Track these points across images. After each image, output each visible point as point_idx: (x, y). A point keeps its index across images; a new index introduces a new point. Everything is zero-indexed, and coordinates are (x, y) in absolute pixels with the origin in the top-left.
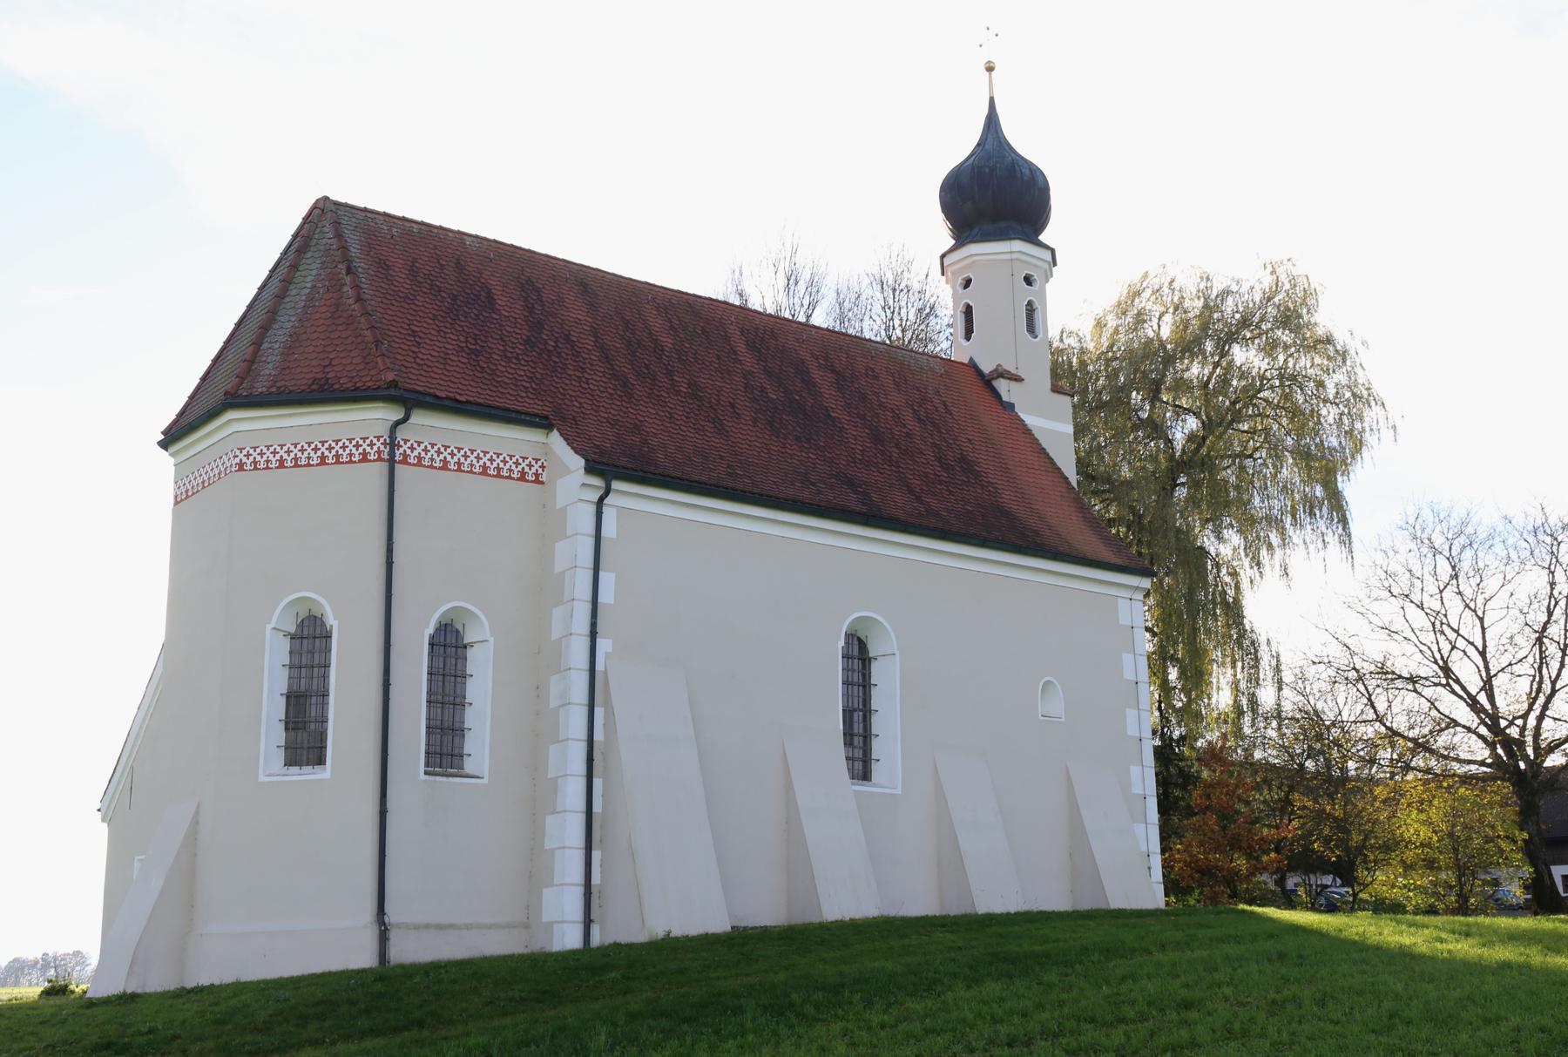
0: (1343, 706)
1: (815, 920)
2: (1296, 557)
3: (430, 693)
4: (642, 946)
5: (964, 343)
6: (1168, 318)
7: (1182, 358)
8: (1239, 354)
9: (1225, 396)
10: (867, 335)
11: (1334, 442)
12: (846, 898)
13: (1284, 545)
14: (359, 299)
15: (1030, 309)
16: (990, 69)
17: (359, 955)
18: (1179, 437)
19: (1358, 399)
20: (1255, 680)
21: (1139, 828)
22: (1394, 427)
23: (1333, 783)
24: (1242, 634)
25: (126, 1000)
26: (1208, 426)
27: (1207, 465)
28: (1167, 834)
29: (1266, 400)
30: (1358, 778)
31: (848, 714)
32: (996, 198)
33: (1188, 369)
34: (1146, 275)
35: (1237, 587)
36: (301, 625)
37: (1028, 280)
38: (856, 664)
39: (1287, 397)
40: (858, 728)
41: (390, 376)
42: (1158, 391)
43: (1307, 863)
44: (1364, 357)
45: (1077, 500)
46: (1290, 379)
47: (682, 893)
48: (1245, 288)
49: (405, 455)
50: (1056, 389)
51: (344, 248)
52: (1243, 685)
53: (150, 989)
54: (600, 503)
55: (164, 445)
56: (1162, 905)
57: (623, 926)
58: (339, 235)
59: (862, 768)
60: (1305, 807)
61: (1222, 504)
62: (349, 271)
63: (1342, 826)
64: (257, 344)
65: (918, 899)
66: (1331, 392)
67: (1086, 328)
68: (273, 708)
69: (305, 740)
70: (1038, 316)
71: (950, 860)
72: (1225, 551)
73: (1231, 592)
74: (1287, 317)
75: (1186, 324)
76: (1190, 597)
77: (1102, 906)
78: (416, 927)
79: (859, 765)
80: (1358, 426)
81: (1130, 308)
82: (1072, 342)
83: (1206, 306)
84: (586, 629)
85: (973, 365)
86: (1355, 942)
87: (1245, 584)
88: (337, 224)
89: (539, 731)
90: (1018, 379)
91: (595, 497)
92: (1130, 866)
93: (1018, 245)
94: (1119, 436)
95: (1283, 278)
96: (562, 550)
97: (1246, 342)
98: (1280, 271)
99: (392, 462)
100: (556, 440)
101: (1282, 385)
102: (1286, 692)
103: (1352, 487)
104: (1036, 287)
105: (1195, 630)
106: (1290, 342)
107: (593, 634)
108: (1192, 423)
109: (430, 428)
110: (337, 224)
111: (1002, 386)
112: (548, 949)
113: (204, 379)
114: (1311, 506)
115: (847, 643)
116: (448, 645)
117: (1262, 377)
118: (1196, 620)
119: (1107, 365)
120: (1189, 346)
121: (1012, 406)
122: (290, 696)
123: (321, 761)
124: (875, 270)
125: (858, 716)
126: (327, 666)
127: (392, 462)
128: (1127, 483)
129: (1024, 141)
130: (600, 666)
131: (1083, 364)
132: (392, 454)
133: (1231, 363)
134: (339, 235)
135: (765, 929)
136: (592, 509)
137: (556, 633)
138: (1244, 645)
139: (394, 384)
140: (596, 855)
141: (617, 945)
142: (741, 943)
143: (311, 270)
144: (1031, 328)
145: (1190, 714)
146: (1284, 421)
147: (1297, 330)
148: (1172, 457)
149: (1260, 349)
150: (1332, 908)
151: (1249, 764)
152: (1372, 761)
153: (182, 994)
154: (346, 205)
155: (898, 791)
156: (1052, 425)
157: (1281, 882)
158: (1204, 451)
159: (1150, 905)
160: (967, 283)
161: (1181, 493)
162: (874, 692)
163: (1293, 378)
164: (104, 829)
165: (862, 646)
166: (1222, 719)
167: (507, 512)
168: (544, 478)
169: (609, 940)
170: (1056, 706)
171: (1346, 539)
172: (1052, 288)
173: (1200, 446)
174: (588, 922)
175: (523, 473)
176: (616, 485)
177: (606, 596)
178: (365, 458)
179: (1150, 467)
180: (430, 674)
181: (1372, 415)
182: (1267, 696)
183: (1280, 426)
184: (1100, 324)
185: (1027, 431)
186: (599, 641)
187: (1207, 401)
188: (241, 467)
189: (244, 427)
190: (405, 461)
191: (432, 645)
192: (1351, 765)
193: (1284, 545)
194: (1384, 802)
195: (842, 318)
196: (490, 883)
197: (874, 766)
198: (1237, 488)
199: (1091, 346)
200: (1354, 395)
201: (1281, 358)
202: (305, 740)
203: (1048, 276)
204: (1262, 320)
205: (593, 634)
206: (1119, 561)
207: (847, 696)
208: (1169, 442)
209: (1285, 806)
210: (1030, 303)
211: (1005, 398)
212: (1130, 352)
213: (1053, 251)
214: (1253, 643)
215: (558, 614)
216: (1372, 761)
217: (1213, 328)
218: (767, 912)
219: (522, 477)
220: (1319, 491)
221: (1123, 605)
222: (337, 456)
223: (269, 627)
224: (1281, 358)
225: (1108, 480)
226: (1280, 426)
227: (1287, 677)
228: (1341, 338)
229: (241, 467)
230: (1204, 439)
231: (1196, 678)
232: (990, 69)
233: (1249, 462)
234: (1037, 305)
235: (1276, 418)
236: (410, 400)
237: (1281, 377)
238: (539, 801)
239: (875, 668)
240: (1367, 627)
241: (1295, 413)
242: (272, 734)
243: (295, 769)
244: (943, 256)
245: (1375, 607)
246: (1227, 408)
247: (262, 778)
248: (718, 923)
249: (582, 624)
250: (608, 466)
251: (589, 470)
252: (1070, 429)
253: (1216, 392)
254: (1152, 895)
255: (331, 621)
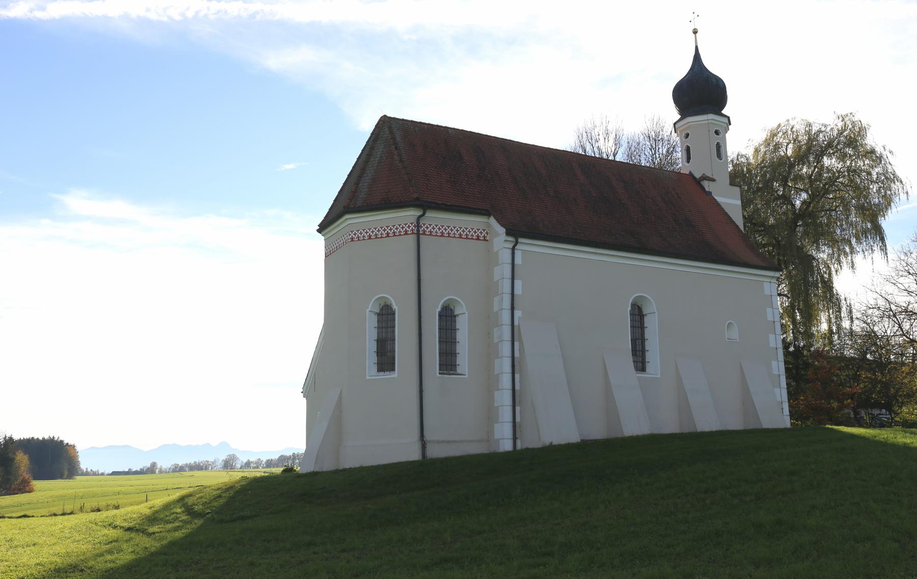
0: (886, 328)
1: (620, 436)
2: (858, 259)
3: (440, 338)
4: (539, 449)
5: (687, 164)
6: (791, 146)
7: (798, 165)
8: (827, 161)
9: (820, 181)
10: (643, 163)
11: (877, 200)
12: (634, 424)
13: (851, 253)
14: (401, 161)
15: (718, 146)
16: (695, 32)
17: (414, 455)
18: (798, 203)
19: (889, 178)
20: (839, 318)
21: (777, 390)
22: (907, 193)
23: (881, 365)
24: (832, 295)
25: (314, 474)
26: (812, 197)
27: (813, 215)
28: (792, 395)
29: (842, 183)
30: (896, 363)
31: (634, 341)
32: (701, 93)
33: (801, 170)
34: (779, 125)
35: (830, 274)
36: (382, 309)
37: (717, 133)
38: (637, 318)
39: (851, 181)
40: (639, 348)
41: (416, 196)
42: (787, 181)
43: (865, 402)
44: (891, 159)
45: (745, 237)
46: (853, 172)
47: (558, 424)
48: (829, 129)
49: (424, 231)
50: (732, 183)
51: (394, 138)
52: (833, 320)
53: (325, 470)
54: (513, 249)
55: (319, 231)
56: (788, 425)
57: (529, 441)
58: (391, 132)
59: (641, 364)
60: (867, 377)
61: (821, 234)
62: (396, 148)
63: (886, 386)
64: (357, 184)
65: (669, 425)
66: (875, 177)
67: (750, 152)
68: (371, 346)
69: (386, 361)
70: (722, 149)
71: (684, 407)
72: (823, 256)
73: (826, 276)
74: (851, 140)
75: (800, 147)
76: (805, 280)
77: (759, 427)
78: (438, 442)
79: (640, 365)
80: (889, 192)
81: (772, 142)
82: (743, 160)
83: (809, 139)
84: (509, 307)
85: (691, 174)
86: (881, 442)
87: (834, 273)
88: (390, 128)
89: (490, 352)
90: (713, 180)
91: (511, 246)
92: (774, 408)
93: (711, 116)
94: (768, 203)
95: (848, 123)
96: (497, 271)
97: (830, 156)
98: (846, 119)
99: (418, 234)
100: (492, 221)
101: (849, 175)
102: (856, 322)
103: (887, 223)
104: (721, 135)
105: (808, 295)
106: (852, 153)
107: (513, 309)
108: (804, 196)
109: (436, 219)
110: (390, 128)
111: (705, 184)
112: (498, 451)
113: (335, 201)
114: (865, 232)
115: (632, 308)
116: (447, 316)
117: (839, 172)
118: (811, 291)
119: (761, 170)
120: (801, 157)
121: (710, 193)
122: (378, 341)
123: (393, 370)
124: (646, 132)
125: (639, 342)
126: (394, 327)
127: (418, 234)
128: (772, 226)
129: (712, 65)
130: (516, 323)
131: (749, 171)
132: (418, 230)
133: (822, 166)
134: (391, 132)
135: (596, 441)
136: (510, 251)
137: (496, 309)
138: (832, 299)
139: (418, 199)
140: (518, 409)
141: (527, 449)
142: (585, 447)
143: (380, 149)
144: (719, 156)
145: (809, 335)
146: (851, 193)
147: (855, 148)
148: (794, 213)
149: (838, 158)
150: (882, 426)
151: (843, 358)
152: (902, 355)
153: (337, 472)
154: (394, 118)
155: (659, 376)
156: (730, 201)
157: (856, 413)
158: (811, 209)
159: (782, 426)
160: (687, 136)
161: (800, 230)
162: (646, 330)
163: (855, 171)
164: (304, 401)
165: (640, 309)
166: (824, 337)
167: (472, 254)
168: (488, 238)
169: (524, 447)
170: (735, 334)
171: (884, 249)
172: (729, 136)
173: (808, 206)
174: (515, 439)
175: (478, 236)
176: (520, 240)
177: (518, 291)
178: (406, 233)
179: (784, 218)
180: (440, 329)
181: (895, 186)
182: (846, 324)
183: (849, 194)
184: (757, 151)
185: (718, 204)
186: (515, 312)
187: (811, 186)
188: (352, 239)
189: (352, 221)
190: (424, 234)
191: (440, 316)
192: (892, 357)
193: (851, 253)
194: (907, 374)
195: (630, 156)
196: (471, 419)
197: (647, 365)
198: (827, 225)
199: (752, 161)
200: (887, 178)
201: (848, 162)
202: (386, 361)
203: (727, 130)
204: (838, 144)
205: (513, 309)
206: (764, 265)
207: (633, 333)
208: (793, 205)
209: (856, 378)
210: (718, 144)
211: (707, 189)
212: (772, 164)
213: (729, 118)
214: (837, 299)
215: (496, 299)
216: (902, 355)
217: (813, 147)
218: (597, 431)
219: (478, 238)
220: (869, 225)
221: (766, 286)
222: (394, 233)
223: (368, 310)
224: (848, 162)
225: (763, 225)
226: (849, 194)
227: (856, 314)
228: (879, 150)
229: (352, 239)
230: (810, 203)
231: (810, 317)
232: (695, 32)
233: (833, 213)
234: (721, 144)
235: (847, 192)
236: (425, 206)
237: (848, 171)
238: (491, 385)
239: (646, 319)
240: (896, 290)
241: (857, 188)
242: (371, 358)
243: (382, 373)
244: (675, 124)
245: (901, 280)
246: (821, 187)
247: (368, 378)
248: (575, 438)
249: (507, 304)
250: (515, 232)
251: (508, 234)
252: (739, 203)
253: (816, 180)
254: (784, 421)
255: (395, 307)
